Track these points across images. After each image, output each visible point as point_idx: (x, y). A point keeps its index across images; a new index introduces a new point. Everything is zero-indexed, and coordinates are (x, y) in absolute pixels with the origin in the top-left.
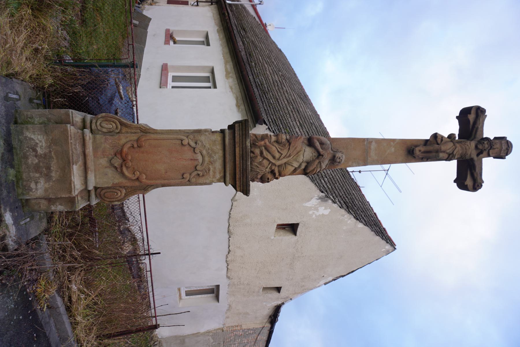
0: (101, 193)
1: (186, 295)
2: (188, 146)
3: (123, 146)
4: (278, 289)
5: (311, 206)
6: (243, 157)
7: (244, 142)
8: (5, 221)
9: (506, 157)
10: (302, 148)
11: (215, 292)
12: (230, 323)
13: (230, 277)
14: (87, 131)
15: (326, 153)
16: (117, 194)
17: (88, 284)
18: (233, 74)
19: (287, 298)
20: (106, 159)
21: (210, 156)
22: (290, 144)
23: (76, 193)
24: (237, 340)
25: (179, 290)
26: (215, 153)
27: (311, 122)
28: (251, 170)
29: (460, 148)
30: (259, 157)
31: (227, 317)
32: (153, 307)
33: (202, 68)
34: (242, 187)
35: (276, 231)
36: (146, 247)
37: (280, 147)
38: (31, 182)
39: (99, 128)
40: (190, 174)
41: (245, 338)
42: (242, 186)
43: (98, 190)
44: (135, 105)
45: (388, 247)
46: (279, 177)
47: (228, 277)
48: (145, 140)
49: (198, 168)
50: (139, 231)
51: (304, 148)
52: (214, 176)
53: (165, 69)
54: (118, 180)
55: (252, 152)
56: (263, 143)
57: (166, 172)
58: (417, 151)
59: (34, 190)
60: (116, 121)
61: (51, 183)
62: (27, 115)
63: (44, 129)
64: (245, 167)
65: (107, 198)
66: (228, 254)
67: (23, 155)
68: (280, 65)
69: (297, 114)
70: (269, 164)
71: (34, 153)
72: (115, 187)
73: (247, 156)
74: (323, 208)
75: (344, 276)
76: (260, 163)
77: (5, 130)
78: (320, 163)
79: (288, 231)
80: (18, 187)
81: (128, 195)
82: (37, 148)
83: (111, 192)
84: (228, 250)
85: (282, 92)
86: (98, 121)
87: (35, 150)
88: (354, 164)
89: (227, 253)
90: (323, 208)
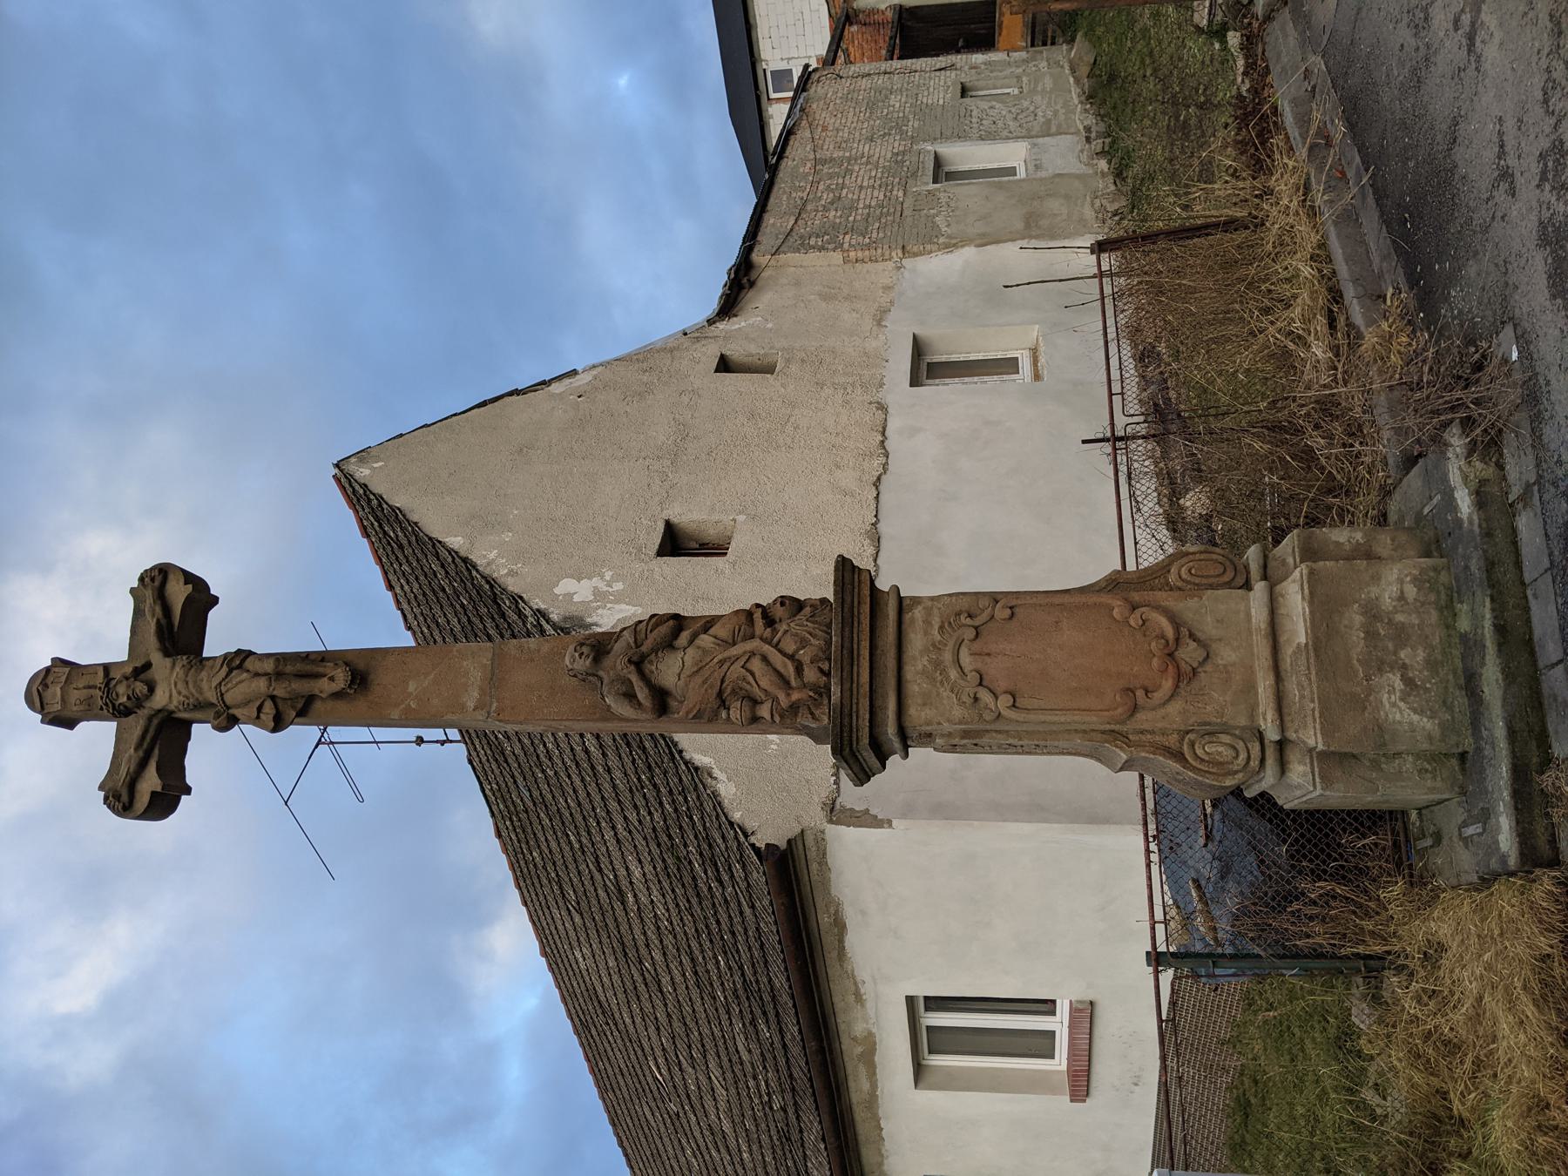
2: (998, 690)
4: (724, 365)
5: (616, 606)
6: (850, 656)
7: (847, 694)
8: (1470, 494)
11: (924, 367)
12: (881, 272)
13: (878, 409)
14: (1272, 735)
15: (620, 668)
16: (1190, 571)
17: (1284, 360)
18: (851, 1051)
19: (697, 338)
20: (1220, 662)
21: (937, 664)
22: (720, 693)
23: (1297, 573)
24: (859, 218)
25: (1037, 377)
26: (924, 672)
27: (577, 919)
28: (829, 626)
29: (205, 685)
30: (806, 660)
31: (888, 288)
32: (1106, 300)
33: (953, 1082)
34: (856, 580)
35: (730, 538)
36: (1121, 458)
37: (748, 687)
38: (1415, 599)
39: (1240, 745)
41: (835, 223)
42: (856, 584)
43: (1240, 580)
44: (1151, 839)
45: (362, 473)
46: (753, 610)
47: (883, 408)
48: (1116, 709)
49: (971, 633)
50: (1139, 499)
51: (681, 683)
52: (929, 611)
53: (1080, 1083)
54: (1188, 607)
56: (795, 696)
58: (341, 678)
59: (1408, 579)
60: (1194, 763)
62: (1434, 778)
64: (847, 629)
65: (1216, 561)
66: (880, 475)
67: (1440, 670)
68: (670, 1149)
69: (628, 940)
70: (780, 641)
71: (1411, 675)
72: (1197, 587)
74: (576, 598)
75: (511, 394)
76: (803, 643)
77: (1483, 729)
79: (692, 538)
80: (1450, 588)
81: (1162, 569)
82: (1402, 687)
83: (1207, 577)
84: (881, 488)
85: (676, 1024)
86: (1244, 763)
87: (1409, 682)
89: (883, 477)
90: (576, 598)
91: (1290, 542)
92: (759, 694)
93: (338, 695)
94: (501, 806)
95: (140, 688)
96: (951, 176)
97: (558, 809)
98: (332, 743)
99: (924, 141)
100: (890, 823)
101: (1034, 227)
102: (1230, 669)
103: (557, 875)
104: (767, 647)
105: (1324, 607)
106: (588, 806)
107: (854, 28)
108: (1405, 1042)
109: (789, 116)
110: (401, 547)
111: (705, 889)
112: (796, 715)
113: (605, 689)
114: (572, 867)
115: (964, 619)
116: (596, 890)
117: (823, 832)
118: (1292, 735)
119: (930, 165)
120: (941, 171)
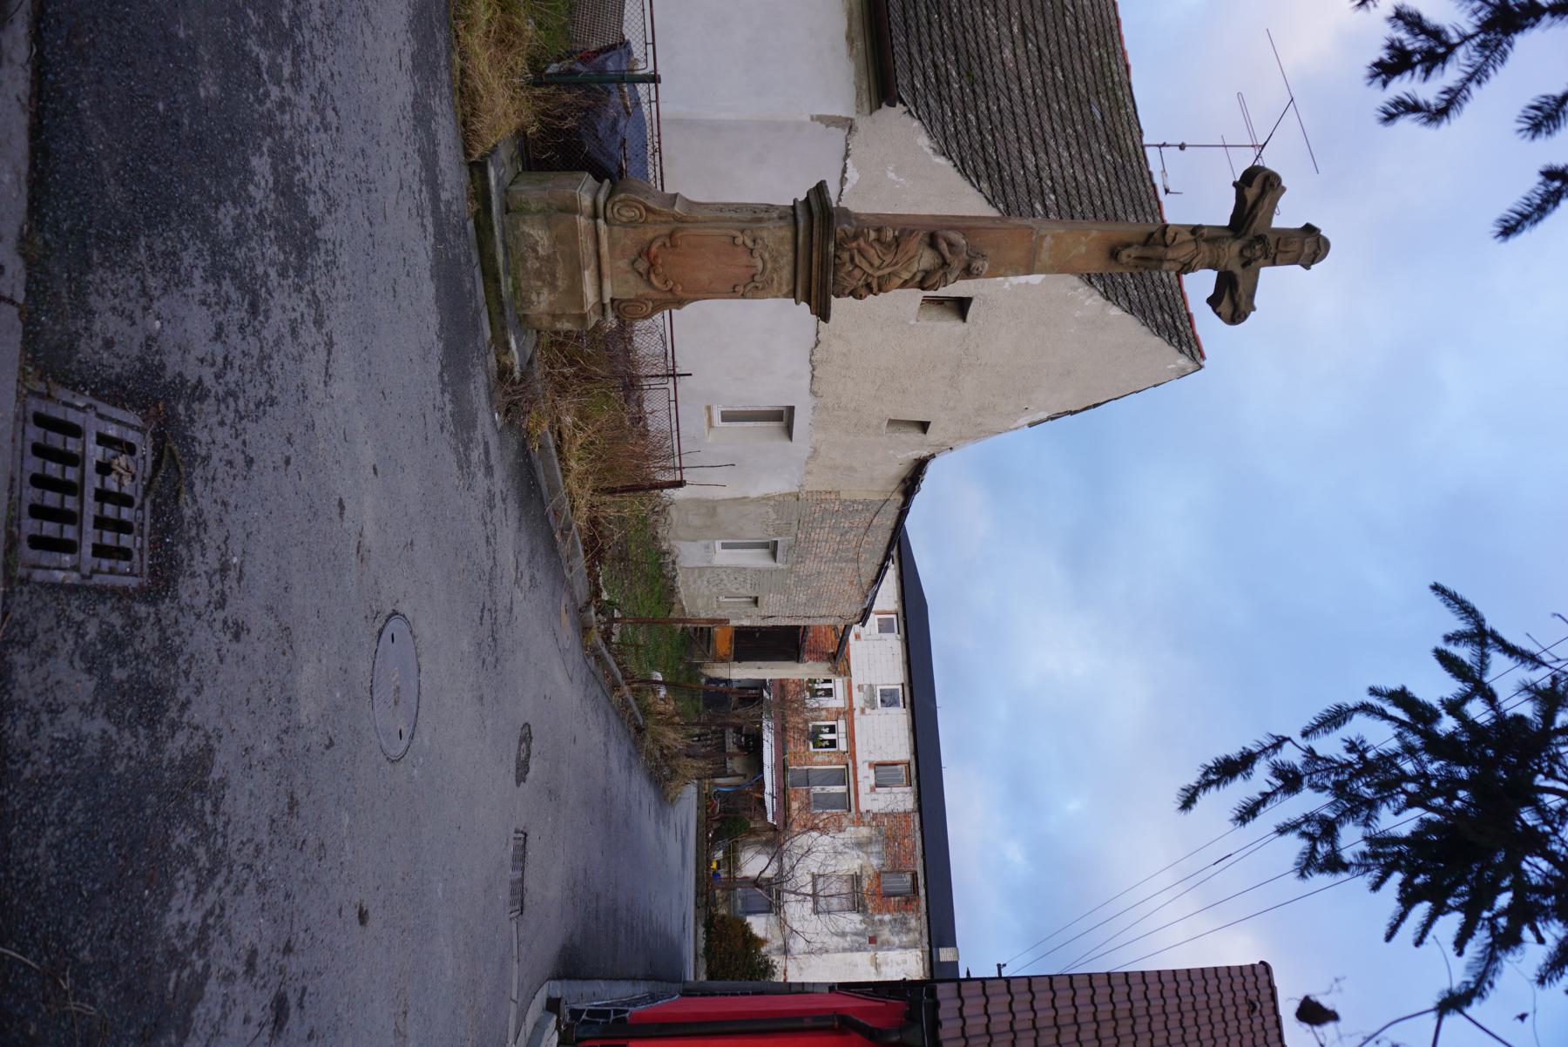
1: (723, 421)
3: (651, 242)
4: (924, 426)
9: (1312, 267)
10: (917, 251)
12: (813, 484)
14: (601, 222)
17: (582, 415)
21: (775, 260)
22: (898, 246)
23: (589, 307)
25: (709, 408)
28: (834, 284)
29: (1207, 254)
31: (809, 473)
36: (670, 364)
40: (745, 287)
43: (616, 303)
47: (813, 393)
49: (757, 278)
52: (779, 290)
56: (854, 244)
72: (639, 300)
75: (1076, 412)
76: (849, 274)
78: (945, 274)
87: (535, 251)
88: (1010, 272)
89: (813, 346)
91: (591, 324)
92: (877, 246)
93: (1128, 245)
94: (1120, 93)
95: (1247, 253)
96: (765, 546)
97: (1068, 98)
98: (1253, 146)
99: (783, 570)
100: (812, 119)
101: (710, 508)
103: (1079, 38)
104: (870, 272)
105: (575, 289)
106: (1042, 106)
107: (831, 651)
108: (523, 40)
109: (876, 592)
110: (1161, 307)
111: (949, 53)
112: (855, 233)
113: (965, 249)
114: (1064, 47)
115: (760, 286)
116: (1046, 30)
117: (858, 112)
118: (591, 221)
119: (779, 554)
120: (772, 549)
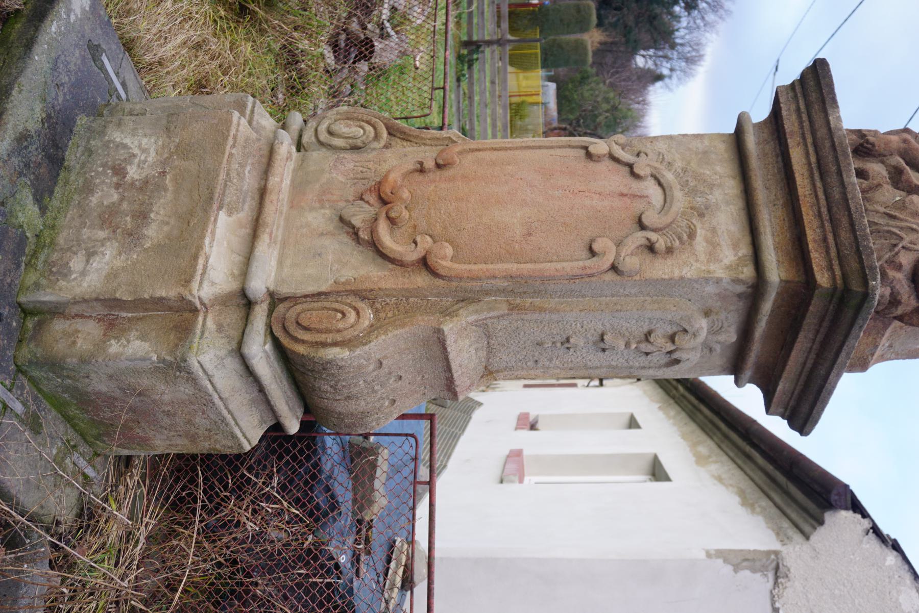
0: (288, 315)
16: (344, 315)
26: (711, 187)
38: (75, 253)
40: (619, 244)
42: (836, 263)
55: (861, 174)
57: (530, 234)
61: (135, 257)
63: (164, 122)
73: (841, 158)
82: (129, 168)
87: (120, 171)
100: (709, 555)
102: (317, 205)
